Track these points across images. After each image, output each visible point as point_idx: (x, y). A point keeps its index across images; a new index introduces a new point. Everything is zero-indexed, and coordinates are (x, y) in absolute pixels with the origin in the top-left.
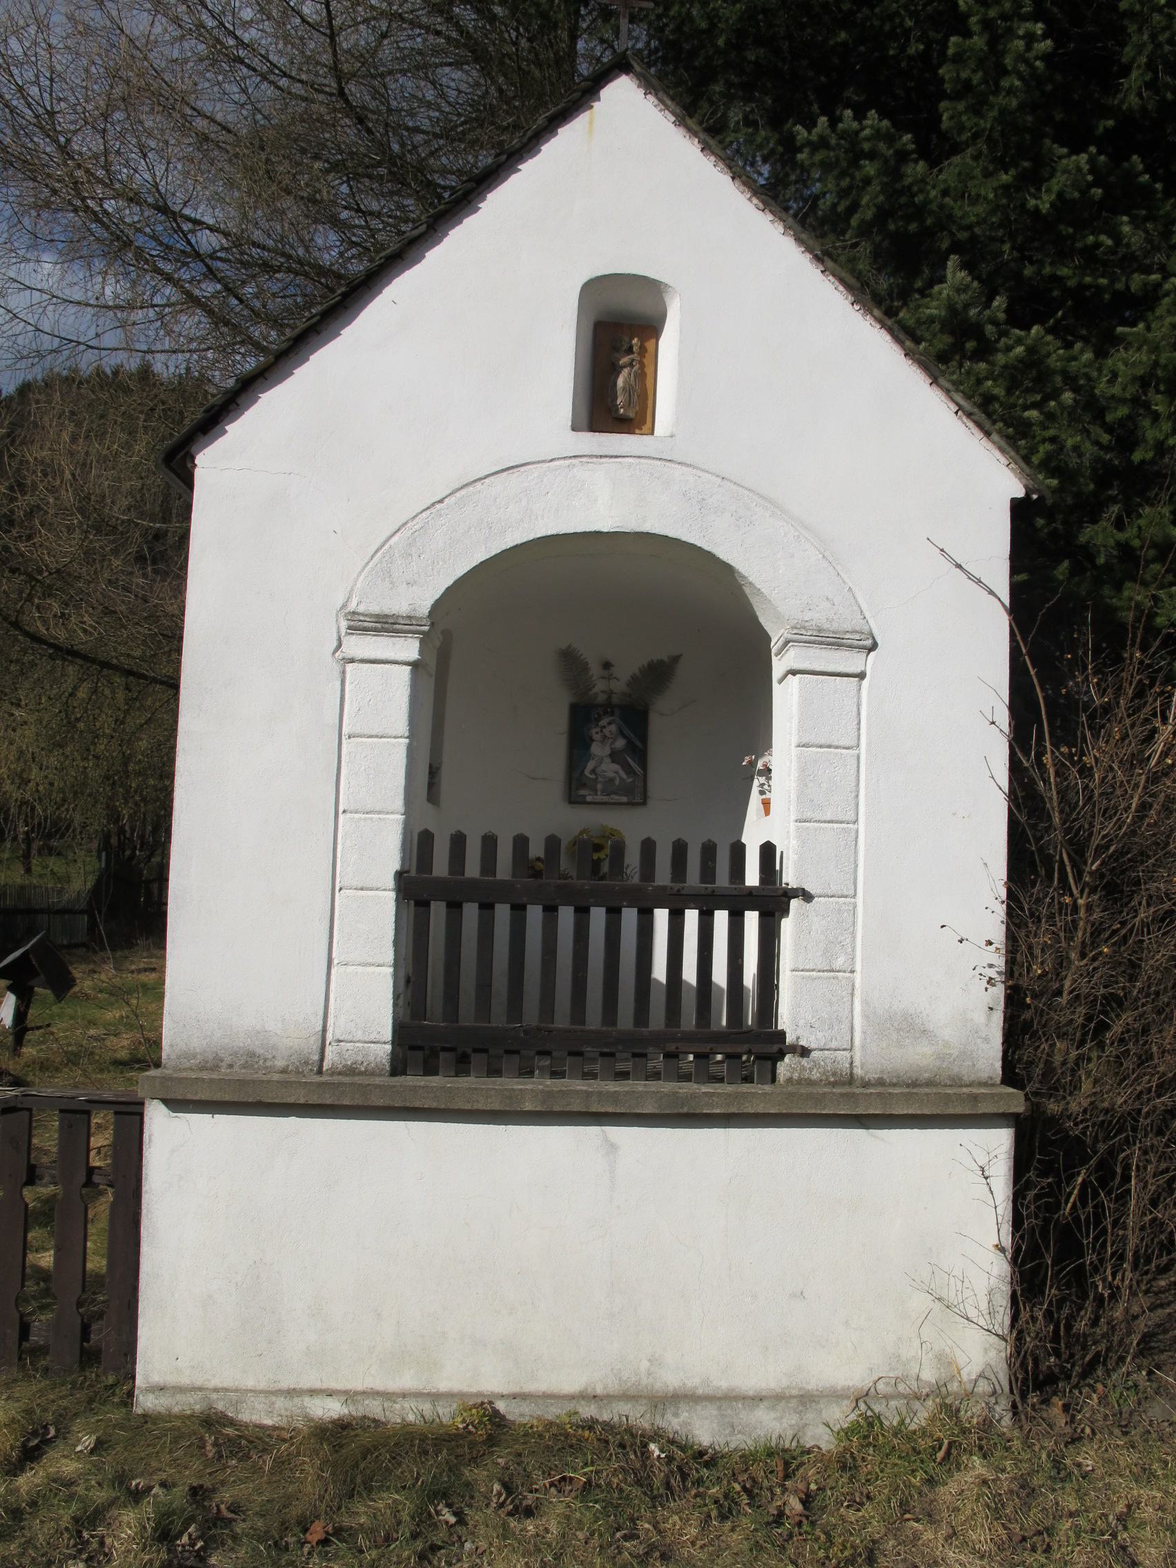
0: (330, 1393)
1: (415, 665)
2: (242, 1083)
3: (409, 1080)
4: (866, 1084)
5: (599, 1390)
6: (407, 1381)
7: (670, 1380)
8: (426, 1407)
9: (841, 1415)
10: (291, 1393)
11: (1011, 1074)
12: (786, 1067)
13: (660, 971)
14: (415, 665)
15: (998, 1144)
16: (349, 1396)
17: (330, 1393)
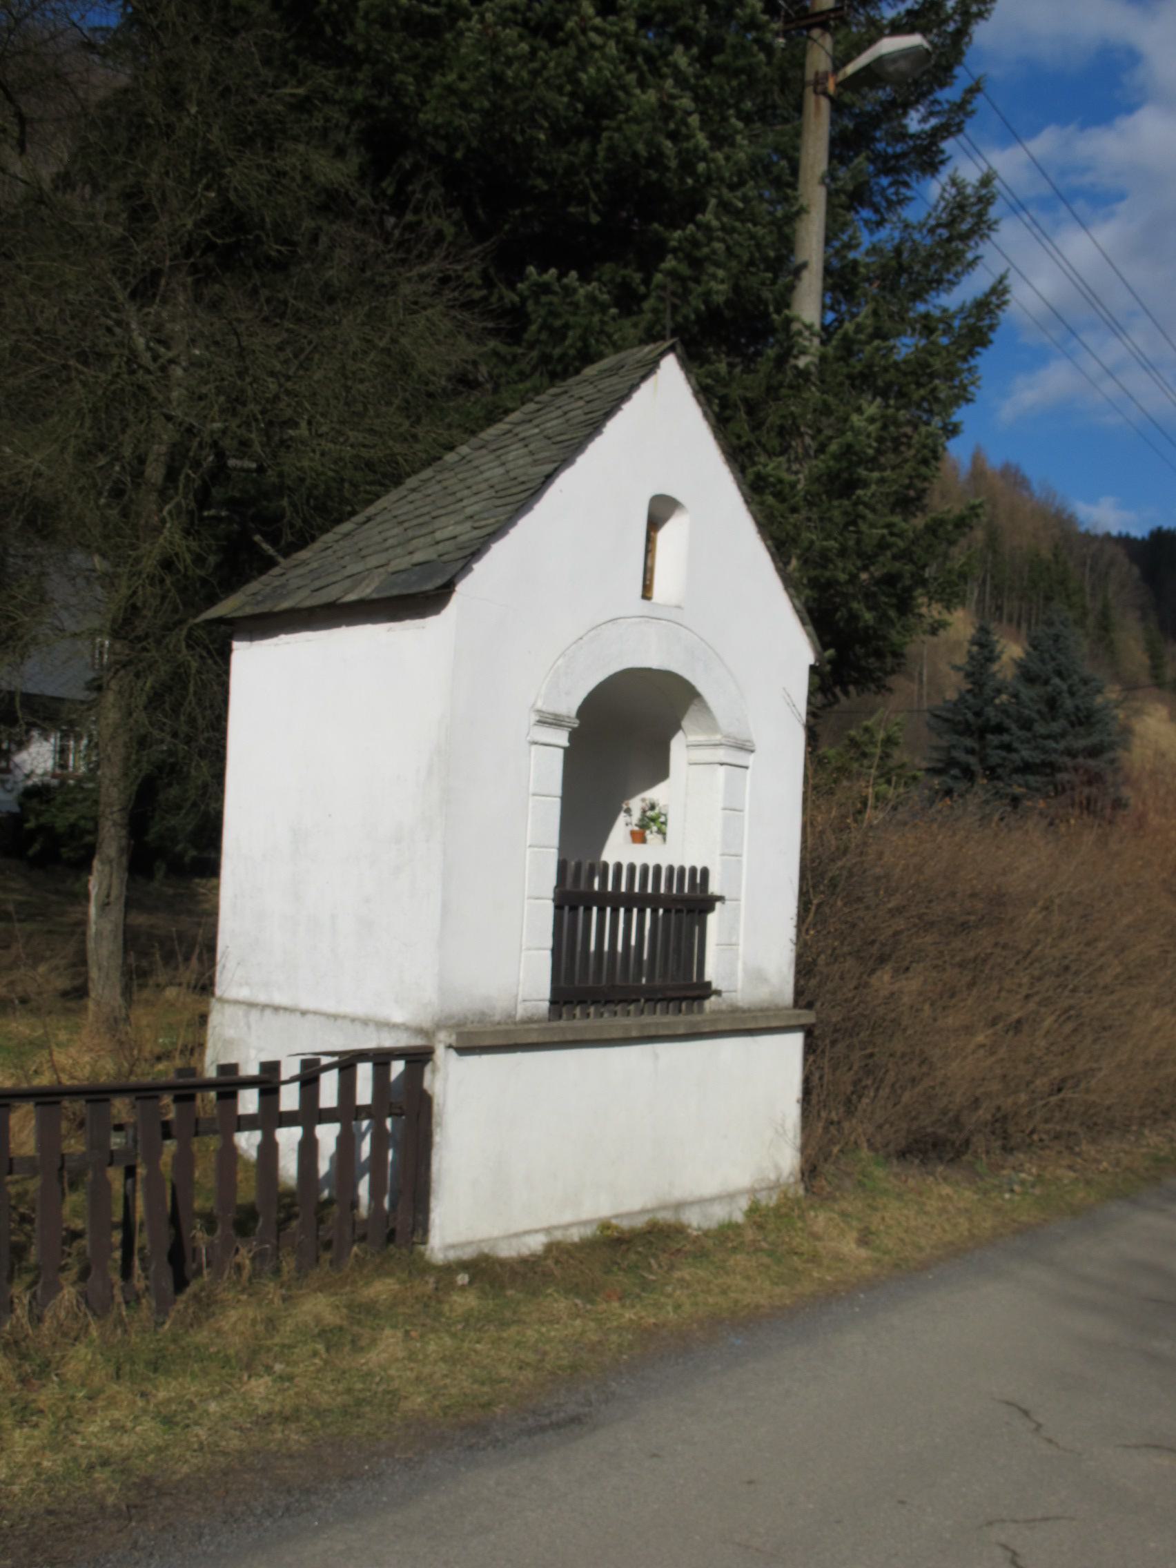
0: (536, 1231)
1: (565, 749)
2: (507, 1032)
3: (562, 1023)
4: (744, 1011)
5: (649, 1206)
6: (567, 1217)
7: (678, 1194)
8: (582, 1230)
9: (744, 1203)
10: (517, 1235)
11: (802, 997)
12: (710, 1004)
13: (593, 947)
14: (565, 749)
15: (795, 1042)
16: (548, 1230)
17: (536, 1231)
